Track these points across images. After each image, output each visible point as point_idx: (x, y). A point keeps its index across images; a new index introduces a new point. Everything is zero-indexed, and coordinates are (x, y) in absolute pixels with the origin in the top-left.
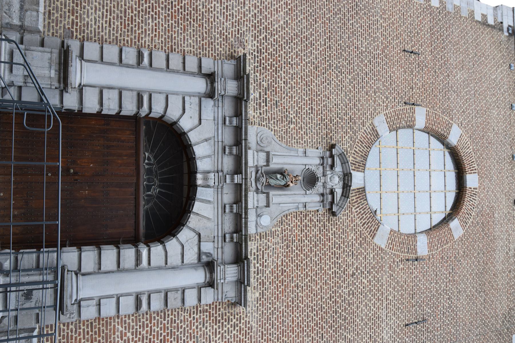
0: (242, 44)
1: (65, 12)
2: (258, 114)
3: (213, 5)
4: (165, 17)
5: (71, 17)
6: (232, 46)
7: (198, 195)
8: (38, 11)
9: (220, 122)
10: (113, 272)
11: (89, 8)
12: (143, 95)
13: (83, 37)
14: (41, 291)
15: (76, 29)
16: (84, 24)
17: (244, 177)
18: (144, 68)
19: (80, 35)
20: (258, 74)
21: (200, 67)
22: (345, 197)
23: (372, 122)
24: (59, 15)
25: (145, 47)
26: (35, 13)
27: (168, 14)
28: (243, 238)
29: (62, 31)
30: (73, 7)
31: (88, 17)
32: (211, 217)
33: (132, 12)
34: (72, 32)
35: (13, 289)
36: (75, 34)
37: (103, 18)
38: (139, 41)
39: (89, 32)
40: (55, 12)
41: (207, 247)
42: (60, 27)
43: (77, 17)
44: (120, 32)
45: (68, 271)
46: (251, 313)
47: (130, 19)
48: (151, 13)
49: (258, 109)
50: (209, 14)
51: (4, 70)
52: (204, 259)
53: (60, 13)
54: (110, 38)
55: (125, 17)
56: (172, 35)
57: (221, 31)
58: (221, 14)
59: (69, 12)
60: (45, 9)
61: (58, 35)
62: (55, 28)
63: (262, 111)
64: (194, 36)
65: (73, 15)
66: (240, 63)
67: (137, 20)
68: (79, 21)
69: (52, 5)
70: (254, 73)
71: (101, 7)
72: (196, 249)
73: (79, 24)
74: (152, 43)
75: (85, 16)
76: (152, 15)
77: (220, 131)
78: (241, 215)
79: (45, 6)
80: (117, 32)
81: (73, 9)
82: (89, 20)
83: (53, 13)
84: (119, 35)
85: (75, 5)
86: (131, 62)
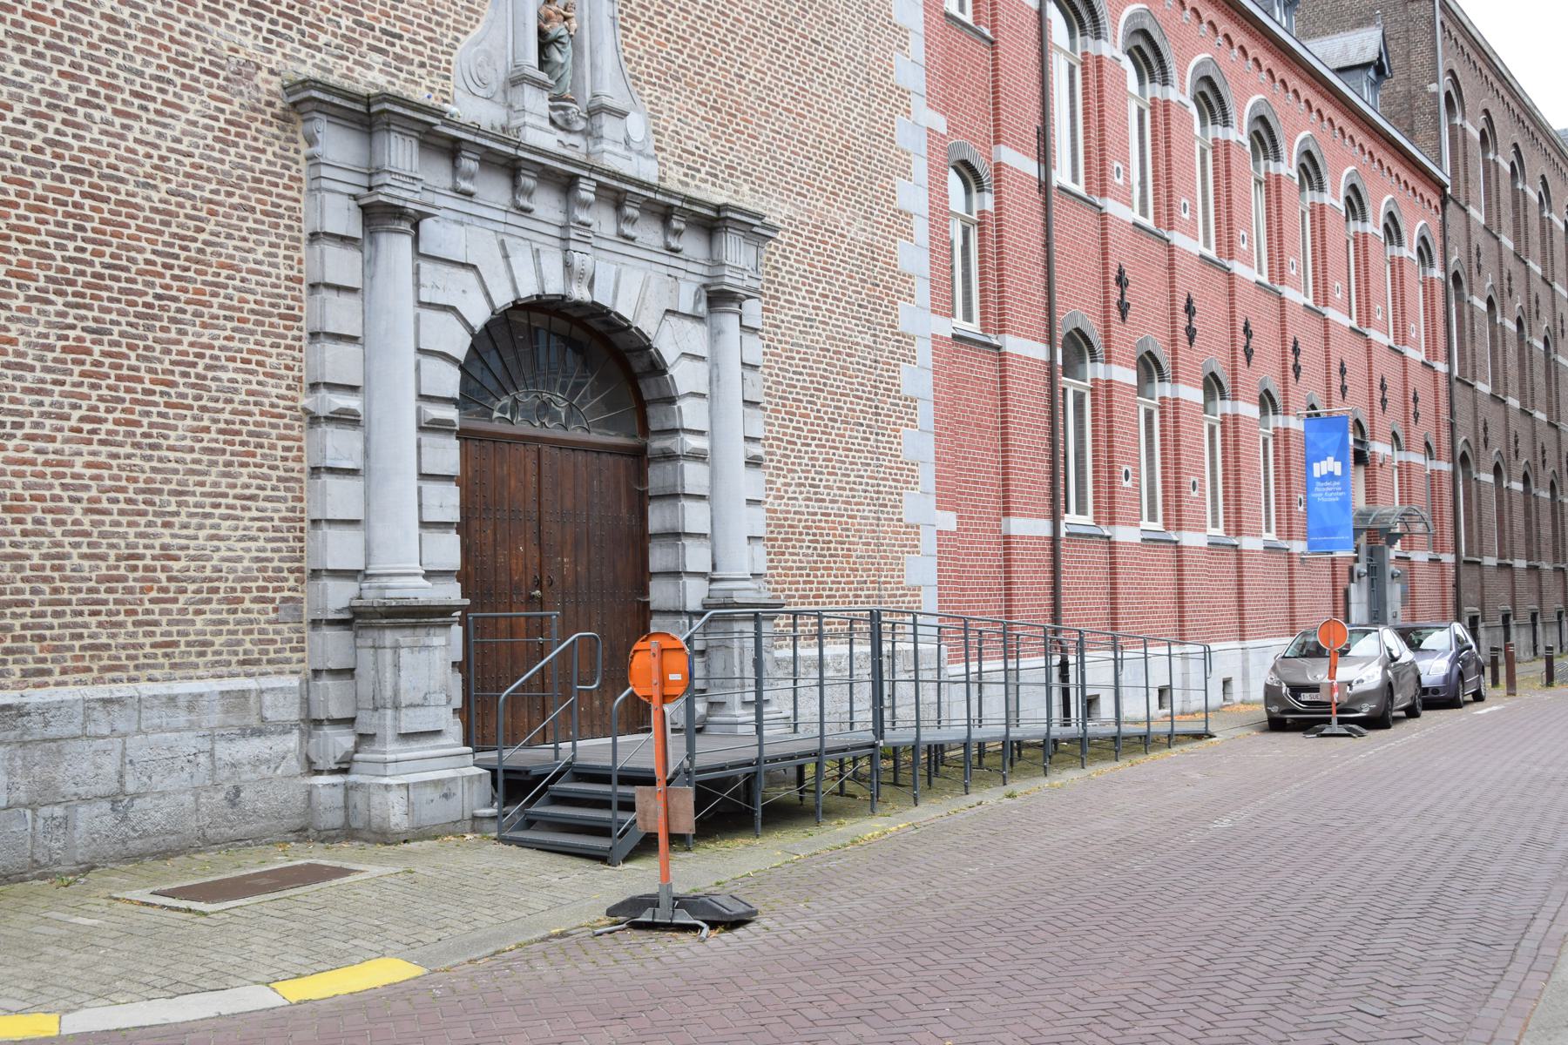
5: (247, 604)
11: (216, 556)
12: (429, 418)
14: (920, 630)
15: (276, 590)
16: (259, 570)
17: (586, 174)
18: (367, 405)
19: (286, 580)
21: (344, 240)
24: (247, 638)
26: (267, 698)
27: (195, 314)
28: (686, 206)
29: (285, 627)
30: (220, 602)
31: (239, 559)
33: (207, 430)
34: (285, 600)
36: (286, 594)
37: (236, 518)
38: (282, 416)
39: (276, 556)
40: (241, 649)
42: (276, 632)
44: (265, 470)
45: (360, 598)
47: (229, 438)
49: (259, 23)
51: (443, 747)
52: (702, 308)
53: (240, 636)
55: (223, 452)
59: (235, 612)
60: (238, 675)
61: (295, 636)
62: (279, 645)
64: (244, 239)
65: (241, 601)
66: (307, 102)
67: (227, 416)
68: (254, 585)
69: (225, 657)
71: (208, 522)
72: (688, 324)
73: (261, 583)
74: (281, 377)
75: (239, 566)
78: (649, 200)
82: (248, 556)
83: (245, 652)
84: (274, 474)
85: (215, 597)
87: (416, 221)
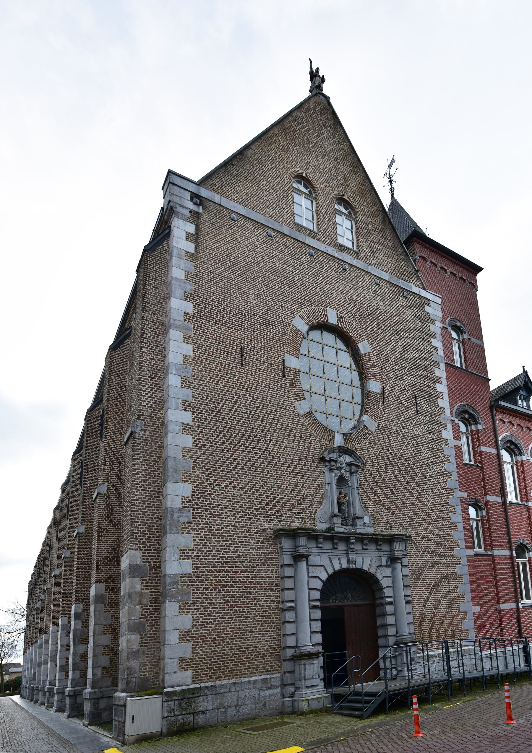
0: (265, 530)
1: (265, 662)
2: (308, 520)
3: (241, 554)
4: (256, 592)
5: (267, 657)
6: (267, 539)
7: (360, 567)
8: (271, 678)
9: (320, 551)
10: (296, 613)
13: (278, 648)
18: (296, 605)
20: (283, 518)
22: (352, 454)
23: (302, 416)
25: (278, 606)
26: (272, 680)
27: (254, 589)
31: (265, 646)
32: (370, 558)
33: (257, 616)
34: (276, 655)
35: (410, 666)
38: (275, 610)
41: (384, 562)
42: (274, 663)
43: (267, 654)
46: (410, 532)
48: (255, 602)
50: (247, 557)
52: (389, 563)
54: (276, 630)
55: (261, 621)
56: (267, 586)
57: (258, 548)
58: (246, 547)
63: (306, 517)
70: (282, 521)
72: (385, 568)
74: (275, 601)
76: (257, 602)
77: (326, 551)
79: (264, 675)
80: (272, 626)
81: (262, 657)
86: (294, 615)
87: (307, 557)
